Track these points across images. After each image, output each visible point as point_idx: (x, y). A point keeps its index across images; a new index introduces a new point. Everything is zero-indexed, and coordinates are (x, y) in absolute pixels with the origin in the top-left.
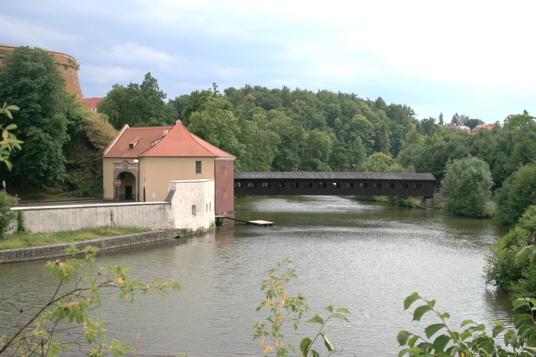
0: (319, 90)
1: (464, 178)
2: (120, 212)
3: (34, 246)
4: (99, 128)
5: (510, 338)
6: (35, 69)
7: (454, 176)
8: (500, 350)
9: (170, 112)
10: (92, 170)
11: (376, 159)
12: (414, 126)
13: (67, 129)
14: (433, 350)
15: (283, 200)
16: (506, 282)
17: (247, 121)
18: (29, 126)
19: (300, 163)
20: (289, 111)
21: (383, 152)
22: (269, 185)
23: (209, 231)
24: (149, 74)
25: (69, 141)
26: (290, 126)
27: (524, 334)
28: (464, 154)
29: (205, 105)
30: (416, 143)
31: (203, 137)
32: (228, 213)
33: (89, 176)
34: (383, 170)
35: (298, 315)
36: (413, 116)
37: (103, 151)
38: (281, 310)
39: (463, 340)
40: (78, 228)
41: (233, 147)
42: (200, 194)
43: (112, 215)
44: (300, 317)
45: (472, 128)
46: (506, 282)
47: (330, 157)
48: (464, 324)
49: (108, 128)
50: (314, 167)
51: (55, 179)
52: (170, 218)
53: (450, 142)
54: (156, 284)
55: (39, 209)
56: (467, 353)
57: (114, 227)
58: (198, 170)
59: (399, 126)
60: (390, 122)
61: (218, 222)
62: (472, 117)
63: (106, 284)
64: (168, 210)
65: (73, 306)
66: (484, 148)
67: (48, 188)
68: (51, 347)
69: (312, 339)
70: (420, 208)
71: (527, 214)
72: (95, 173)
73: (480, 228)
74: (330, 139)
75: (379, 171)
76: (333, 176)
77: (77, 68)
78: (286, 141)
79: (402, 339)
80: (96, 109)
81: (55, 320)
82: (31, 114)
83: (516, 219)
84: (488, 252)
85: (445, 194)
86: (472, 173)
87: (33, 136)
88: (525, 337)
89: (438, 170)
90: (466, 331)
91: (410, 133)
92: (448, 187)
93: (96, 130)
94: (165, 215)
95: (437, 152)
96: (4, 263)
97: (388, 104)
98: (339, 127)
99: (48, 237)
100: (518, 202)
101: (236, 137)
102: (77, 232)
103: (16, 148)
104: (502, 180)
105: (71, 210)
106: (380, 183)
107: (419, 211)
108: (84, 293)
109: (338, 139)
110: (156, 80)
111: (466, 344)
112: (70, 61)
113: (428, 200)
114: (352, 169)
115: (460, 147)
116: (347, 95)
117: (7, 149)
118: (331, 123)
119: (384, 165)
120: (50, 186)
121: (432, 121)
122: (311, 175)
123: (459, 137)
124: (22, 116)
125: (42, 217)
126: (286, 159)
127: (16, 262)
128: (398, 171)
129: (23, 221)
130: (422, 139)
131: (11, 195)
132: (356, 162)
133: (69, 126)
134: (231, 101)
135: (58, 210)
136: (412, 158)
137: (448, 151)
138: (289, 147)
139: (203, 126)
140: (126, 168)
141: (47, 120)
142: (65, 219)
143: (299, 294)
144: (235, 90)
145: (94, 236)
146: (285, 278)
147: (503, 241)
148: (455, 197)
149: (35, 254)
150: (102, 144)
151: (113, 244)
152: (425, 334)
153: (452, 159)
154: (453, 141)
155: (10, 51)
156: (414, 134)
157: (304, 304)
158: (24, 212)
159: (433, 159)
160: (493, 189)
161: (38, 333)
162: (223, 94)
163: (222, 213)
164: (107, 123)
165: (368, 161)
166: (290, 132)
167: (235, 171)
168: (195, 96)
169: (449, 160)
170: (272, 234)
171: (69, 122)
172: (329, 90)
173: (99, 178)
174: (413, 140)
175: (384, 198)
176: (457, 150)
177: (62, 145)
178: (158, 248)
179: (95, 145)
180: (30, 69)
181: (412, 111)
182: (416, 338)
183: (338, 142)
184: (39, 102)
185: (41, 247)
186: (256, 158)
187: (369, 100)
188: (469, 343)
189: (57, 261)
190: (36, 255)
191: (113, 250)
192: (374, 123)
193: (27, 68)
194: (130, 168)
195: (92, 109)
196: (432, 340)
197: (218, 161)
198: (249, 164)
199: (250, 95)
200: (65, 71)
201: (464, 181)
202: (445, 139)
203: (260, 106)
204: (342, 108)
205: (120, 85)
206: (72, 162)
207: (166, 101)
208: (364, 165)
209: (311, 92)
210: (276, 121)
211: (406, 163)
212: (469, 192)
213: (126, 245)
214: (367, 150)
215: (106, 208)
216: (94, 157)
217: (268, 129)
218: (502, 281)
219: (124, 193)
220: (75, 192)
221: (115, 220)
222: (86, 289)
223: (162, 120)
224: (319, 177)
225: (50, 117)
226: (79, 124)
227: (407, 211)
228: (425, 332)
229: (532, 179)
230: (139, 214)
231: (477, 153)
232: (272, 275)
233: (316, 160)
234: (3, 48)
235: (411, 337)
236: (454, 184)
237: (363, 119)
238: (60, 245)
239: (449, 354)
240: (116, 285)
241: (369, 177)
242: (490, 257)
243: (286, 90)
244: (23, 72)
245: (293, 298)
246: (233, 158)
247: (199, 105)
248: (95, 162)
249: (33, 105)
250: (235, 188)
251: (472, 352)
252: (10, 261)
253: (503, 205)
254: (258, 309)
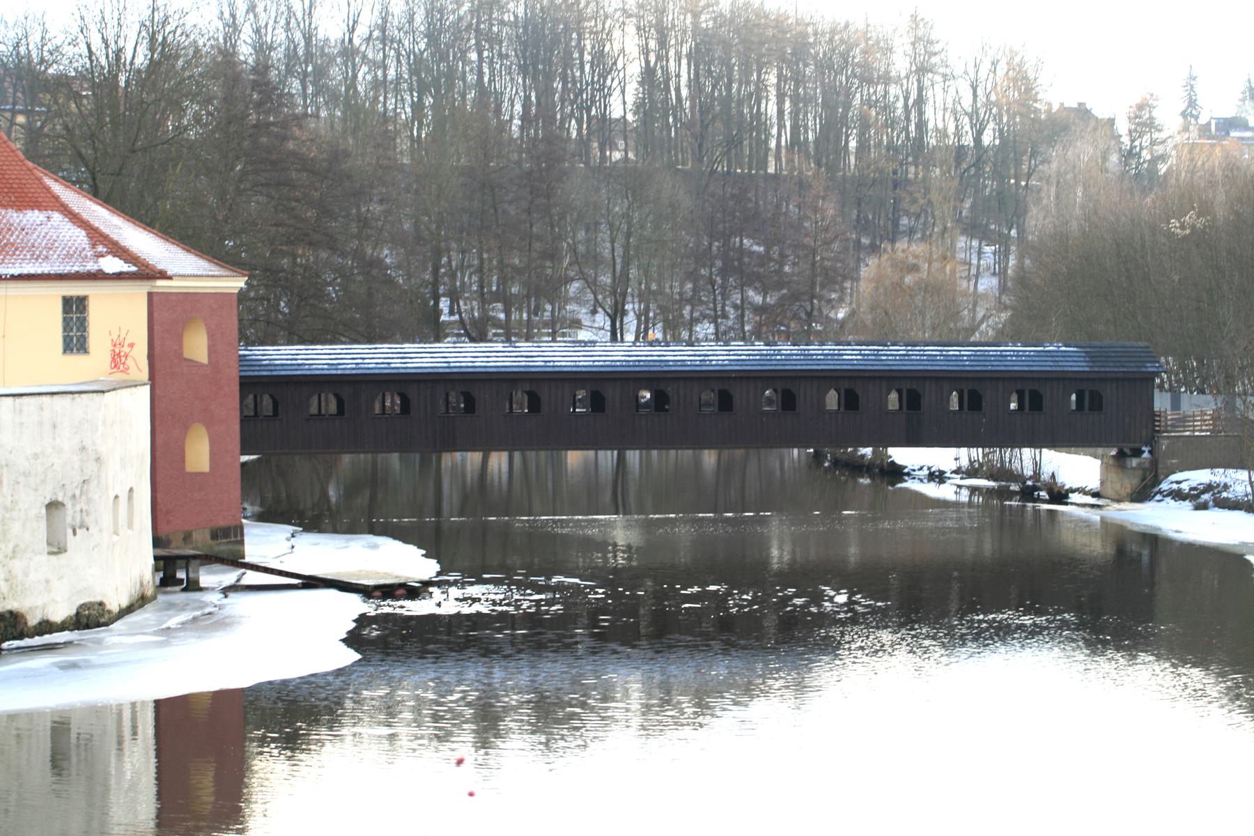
197: (166, 296)
213: (1013, 503)
250: (244, 420)
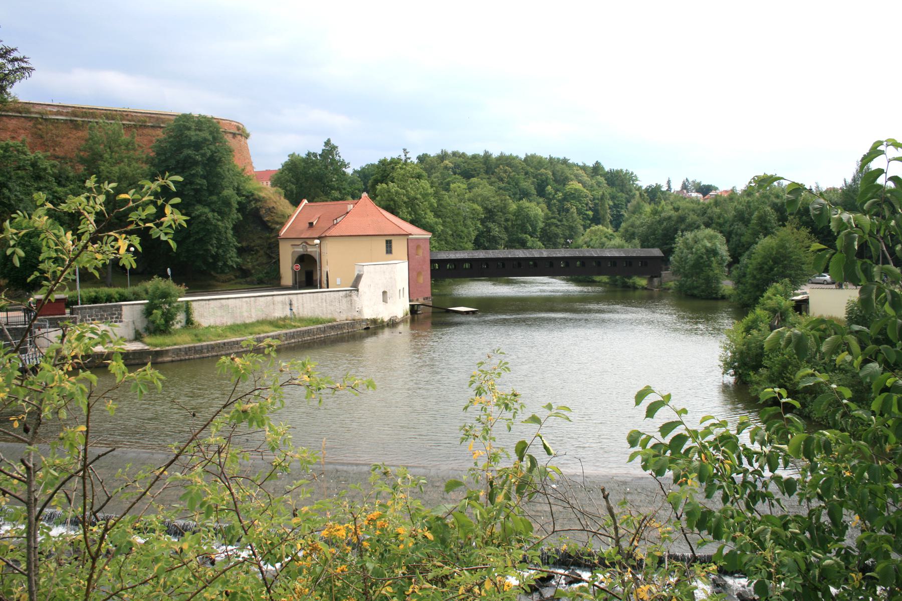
0: (526, 154)
1: (696, 253)
2: (300, 301)
3: (204, 341)
4: (274, 205)
5: (756, 435)
6: (200, 139)
7: (685, 251)
8: (746, 449)
9: (355, 183)
10: (267, 254)
11: (595, 233)
12: (637, 193)
13: (237, 206)
14: (669, 452)
15: (489, 283)
16: (745, 372)
17: (444, 192)
18: (194, 205)
19: (507, 239)
20: (493, 179)
21: (603, 225)
22: (471, 266)
23: (403, 321)
24: (329, 140)
25: (240, 221)
26: (494, 197)
27: (772, 430)
28: (696, 226)
29: (395, 175)
30: (641, 213)
31: (393, 212)
33: (264, 260)
34: (602, 245)
35: (512, 414)
36: (637, 183)
37: (279, 230)
38: (493, 409)
39: (703, 439)
40: (254, 320)
41: (428, 222)
42: (391, 278)
43: (291, 304)
44: (514, 417)
45: (704, 195)
46: (745, 372)
47: (541, 232)
48: (704, 419)
49: (284, 205)
50: (523, 245)
51: (225, 264)
52: (358, 306)
53: (680, 211)
54: (346, 384)
55: (209, 300)
56: (708, 454)
57: (293, 318)
59: (620, 194)
60: (609, 190)
61: (413, 310)
62: (705, 182)
63: (289, 383)
64: (355, 297)
65: (252, 408)
66: (719, 218)
67: (218, 275)
68: (229, 456)
69: (528, 442)
70: (646, 289)
71: (768, 294)
72: (270, 257)
73: (714, 310)
74: (540, 210)
75: (599, 247)
76: (545, 254)
77: (247, 136)
78: (490, 214)
79: (633, 439)
80: (269, 183)
81: (232, 423)
82: (196, 191)
83: (756, 301)
84: (724, 338)
85: (675, 273)
86: (705, 247)
87: (199, 216)
88: (774, 433)
89: (667, 244)
90: (707, 428)
91: (634, 202)
92: (677, 264)
93: (271, 206)
94: (351, 303)
95: (665, 224)
96: (172, 361)
97: (607, 169)
98: (551, 197)
99: (220, 331)
100: (758, 280)
101: (431, 211)
102: (252, 325)
103: (180, 225)
104: (740, 255)
105: (244, 299)
106: (599, 260)
107: (645, 293)
108: (264, 393)
109: (550, 210)
110: (337, 147)
111: (707, 444)
112: (238, 128)
113: (655, 279)
114: (566, 245)
115: (692, 217)
116: (558, 159)
117: (170, 226)
118: (541, 192)
119: (604, 239)
120: (221, 273)
121: (658, 187)
122: (520, 253)
123: (692, 206)
124: (186, 193)
125: (213, 308)
126: (490, 235)
127: (185, 360)
128: (620, 247)
129: (191, 314)
130: (648, 208)
131: (178, 285)
132: (571, 237)
133: (239, 203)
134: (425, 169)
135: (230, 300)
136: (636, 231)
137: (677, 222)
138: (494, 222)
139: (393, 200)
141: (214, 198)
142: (238, 311)
143: (513, 390)
144: (429, 156)
145: (272, 329)
146: (496, 372)
147: (741, 326)
148: (686, 276)
149: (205, 350)
150: (277, 223)
151: (293, 337)
152: (660, 433)
153: (682, 231)
154: (684, 210)
155: (171, 120)
156: (638, 203)
157: (519, 402)
158: (192, 303)
159: (660, 231)
160: (730, 265)
161: (214, 439)
162: (416, 161)
163: (417, 300)
164: (282, 198)
165: (586, 236)
166: (495, 204)
167: (431, 251)
168: (383, 165)
169: (680, 233)
170: (475, 323)
171: (239, 199)
172: (538, 154)
173: (275, 263)
174: (637, 210)
175: (605, 279)
176: (689, 220)
177: (232, 225)
178: (345, 342)
179: (270, 224)
180: (193, 139)
181: (636, 176)
182: (649, 438)
183: (550, 214)
184: (204, 177)
185: (212, 343)
186: (454, 234)
187: (585, 164)
188: (710, 443)
189: (232, 356)
190: (208, 351)
191: (293, 345)
192: (591, 191)
193: (190, 138)
194: (310, 250)
195: (265, 183)
196: (667, 440)
197: (412, 239)
198: (447, 242)
199: (447, 162)
200: (233, 140)
201: (696, 256)
202: (674, 208)
203: (459, 174)
204: (554, 174)
205: (297, 154)
206: (244, 244)
207: (349, 171)
208: (580, 240)
209: (517, 157)
210: (477, 192)
211: (629, 237)
212: (702, 270)
213: (309, 338)
214: (583, 223)
215: (284, 296)
216: (269, 238)
217: (469, 200)
218: (740, 371)
219: (304, 279)
220: (248, 279)
221: (294, 310)
222: (152, 485)
223: (345, 194)
224: (528, 255)
225: (218, 194)
226: (251, 201)
227: (631, 293)
228: (659, 431)
229: (774, 253)
230: (322, 302)
231: (711, 224)
232: (480, 369)
233: (525, 236)
234: (163, 117)
235: (644, 437)
236: (685, 260)
237: (577, 187)
238: (234, 339)
239: (687, 456)
240: (301, 383)
241: (587, 254)
242: (727, 344)
243: (487, 156)
244: (186, 143)
245: (507, 395)
246: (428, 235)
247: (388, 175)
248: (270, 244)
249: (198, 181)
250: (431, 270)
251: (714, 452)
252: (179, 358)
253: (742, 284)
254: (466, 408)
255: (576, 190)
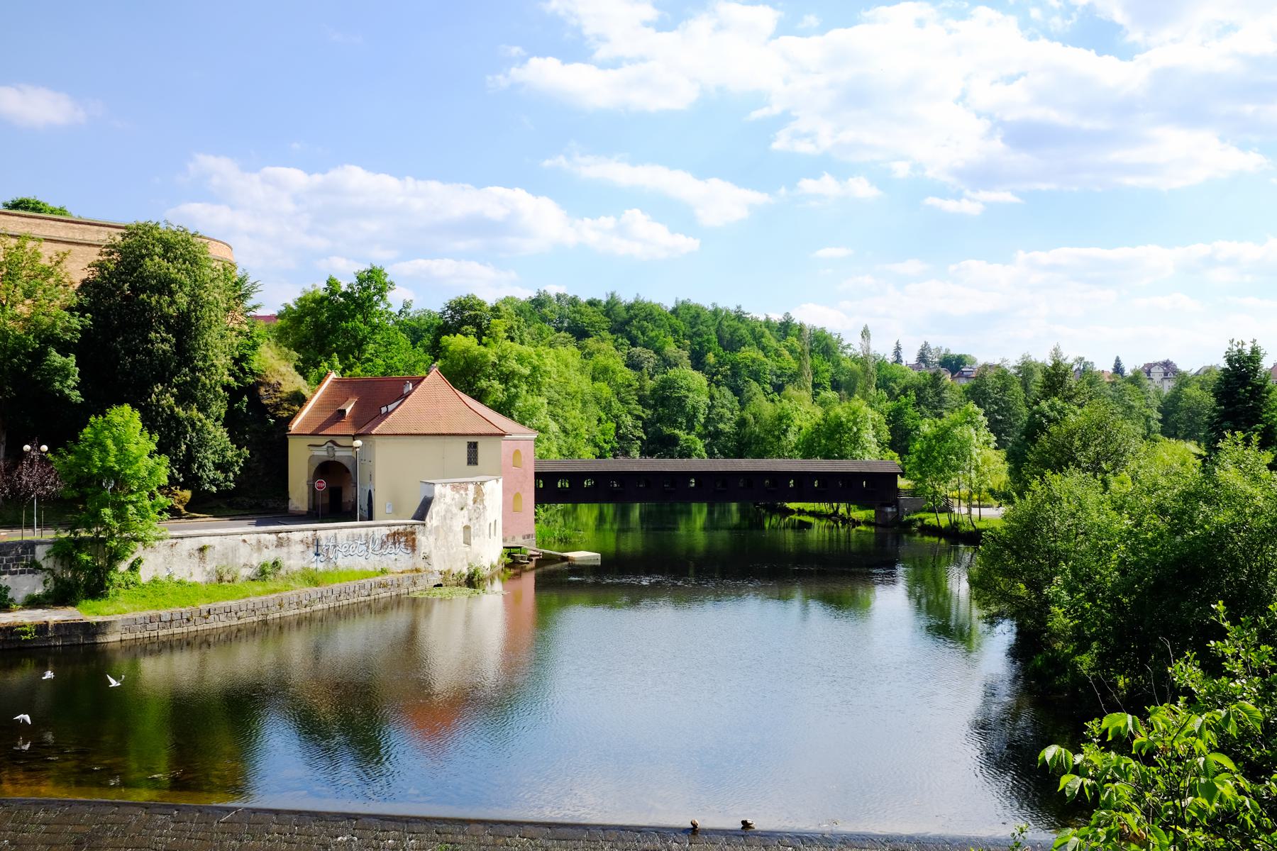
32: (524, 538)
58: (473, 459)
140: (331, 453)
255: (753, 361)
